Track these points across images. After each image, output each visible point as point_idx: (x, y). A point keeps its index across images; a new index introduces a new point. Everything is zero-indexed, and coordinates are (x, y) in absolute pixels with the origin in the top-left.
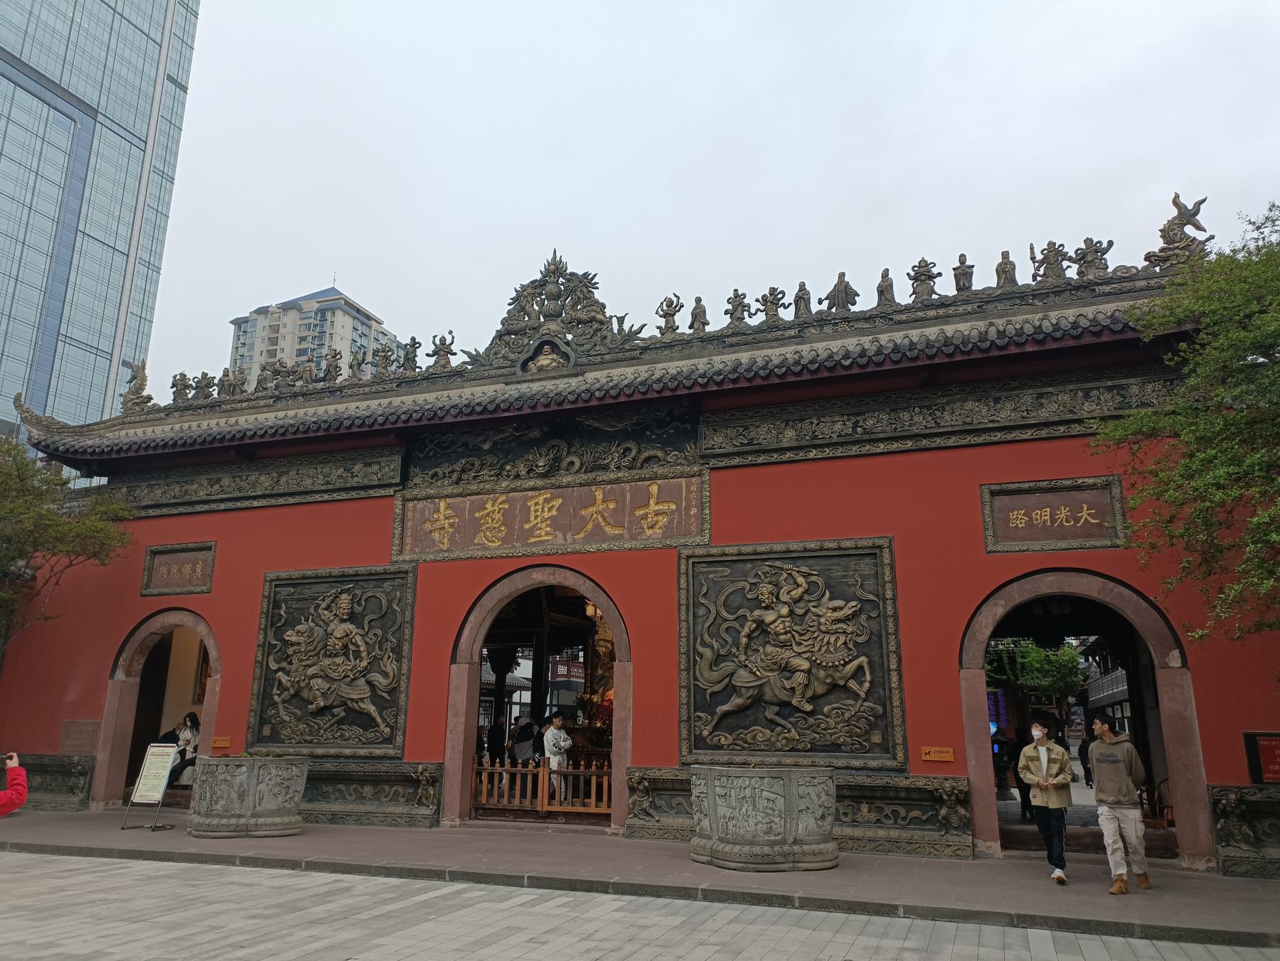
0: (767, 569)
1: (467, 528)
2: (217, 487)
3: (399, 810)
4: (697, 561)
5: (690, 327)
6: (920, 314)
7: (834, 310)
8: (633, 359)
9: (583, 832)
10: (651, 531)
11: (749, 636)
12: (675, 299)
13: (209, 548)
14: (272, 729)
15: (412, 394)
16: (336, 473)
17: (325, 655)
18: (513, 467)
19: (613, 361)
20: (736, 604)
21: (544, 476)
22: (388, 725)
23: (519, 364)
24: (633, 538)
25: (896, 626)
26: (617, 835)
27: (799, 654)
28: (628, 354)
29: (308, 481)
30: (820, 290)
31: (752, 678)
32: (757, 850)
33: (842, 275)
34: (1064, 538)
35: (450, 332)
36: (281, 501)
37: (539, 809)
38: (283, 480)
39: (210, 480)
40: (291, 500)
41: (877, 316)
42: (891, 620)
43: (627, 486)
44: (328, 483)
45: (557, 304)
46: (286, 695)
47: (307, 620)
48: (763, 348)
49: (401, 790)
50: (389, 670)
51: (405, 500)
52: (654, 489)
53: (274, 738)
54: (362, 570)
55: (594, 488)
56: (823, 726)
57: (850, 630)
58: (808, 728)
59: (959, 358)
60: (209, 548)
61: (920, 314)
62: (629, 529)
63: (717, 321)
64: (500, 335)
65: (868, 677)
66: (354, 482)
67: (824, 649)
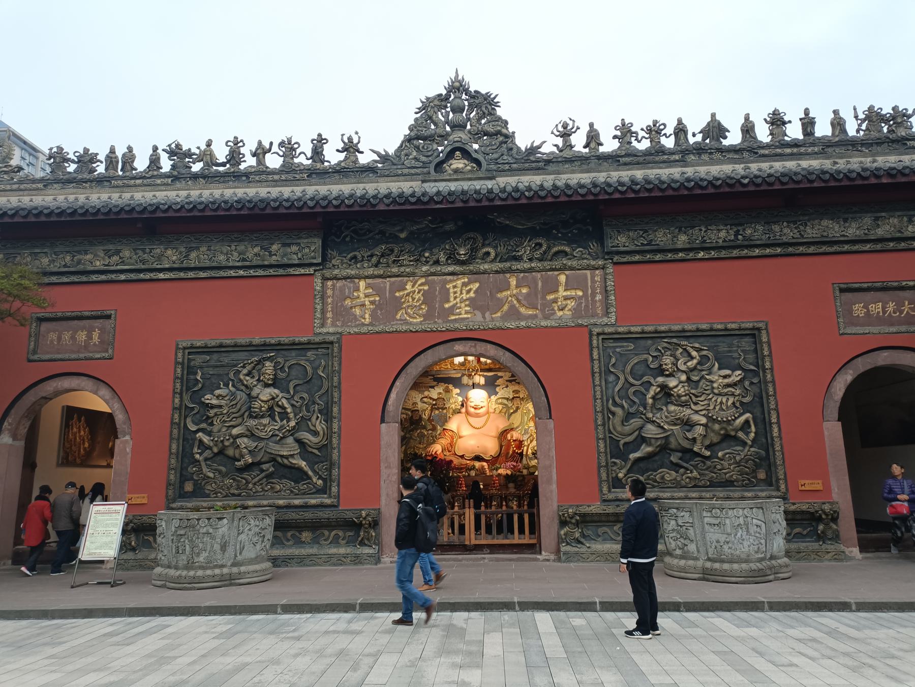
0: (665, 345)
1: (388, 306)
2: (115, 258)
3: (342, 551)
4: (606, 337)
5: (585, 147)
6: (779, 151)
7: (708, 141)
8: (539, 169)
9: (518, 560)
10: (561, 313)
11: (653, 398)
12: (571, 123)
13: (108, 317)
14: (194, 485)
15: (325, 184)
16: (253, 252)
17: (250, 416)
18: (431, 254)
19: (520, 170)
20: (640, 373)
21: (463, 263)
22: (320, 478)
23: (432, 166)
24: (546, 318)
25: (774, 389)
26: (548, 560)
27: (697, 412)
28: (534, 165)
29: (222, 257)
30: (695, 126)
31: (660, 431)
32: (753, 566)
33: (713, 115)
34: (892, 325)
35: (357, 133)
36: (191, 274)
37: (467, 543)
38: (193, 255)
39: (106, 252)
40: (202, 274)
41: (744, 149)
42: (770, 385)
43: (539, 275)
44: (244, 260)
45: (460, 119)
46: (207, 453)
47: (227, 385)
48: (652, 168)
49: (341, 533)
50: (319, 428)
51: (325, 279)
52: (562, 278)
53: (199, 492)
54: (285, 340)
55: (508, 275)
56: (719, 467)
57: (738, 392)
58: (707, 469)
59: (833, 184)
60: (108, 317)
61: (779, 151)
62: (542, 311)
63: (333, 156)
64: (409, 140)
65: (753, 428)
66: (273, 260)
67: (718, 408)
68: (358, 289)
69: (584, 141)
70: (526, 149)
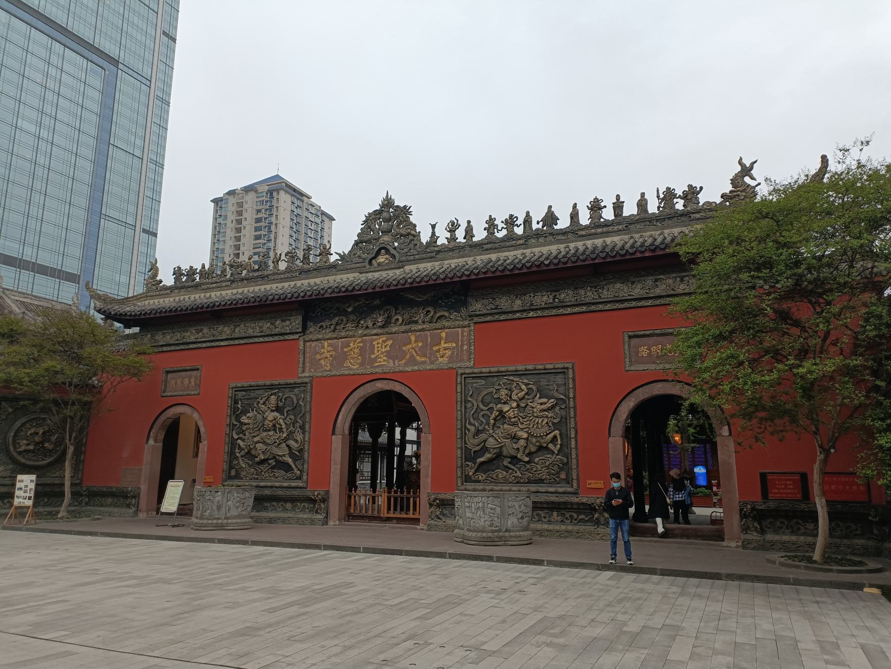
2: (201, 334)
3: (305, 516)
4: (466, 376)
6: (593, 231)
11: (495, 419)
16: (266, 326)
17: (264, 431)
23: (367, 261)
24: (432, 363)
25: (575, 413)
29: (251, 331)
30: (538, 216)
32: (484, 535)
36: (236, 342)
38: (237, 330)
39: (197, 330)
43: (428, 333)
44: (262, 332)
49: (306, 505)
50: (298, 438)
52: (443, 335)
53: (237, 476)
57: (550, 415)
60: (198, 369)
61: (593, 231)
62: (430, 358)
64: (357, 243)
66: (277, 331)
68: (323, 348)
69: (464, 234)
70: (427, 243)
